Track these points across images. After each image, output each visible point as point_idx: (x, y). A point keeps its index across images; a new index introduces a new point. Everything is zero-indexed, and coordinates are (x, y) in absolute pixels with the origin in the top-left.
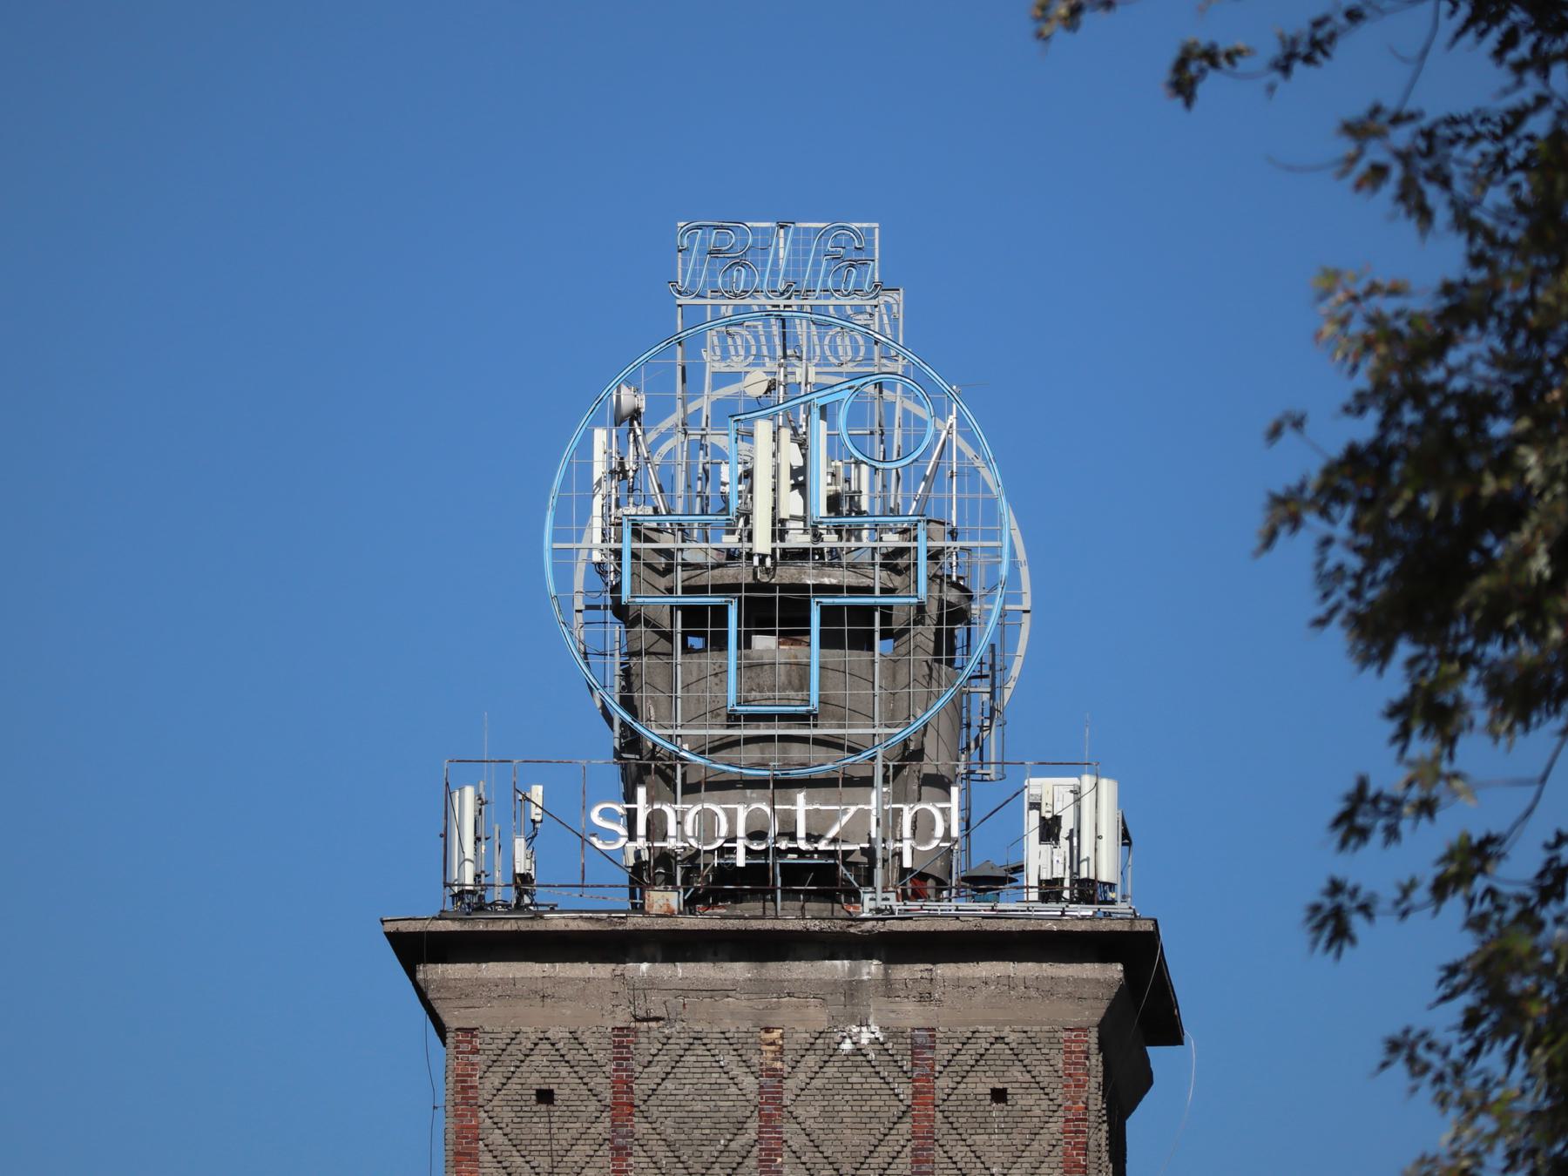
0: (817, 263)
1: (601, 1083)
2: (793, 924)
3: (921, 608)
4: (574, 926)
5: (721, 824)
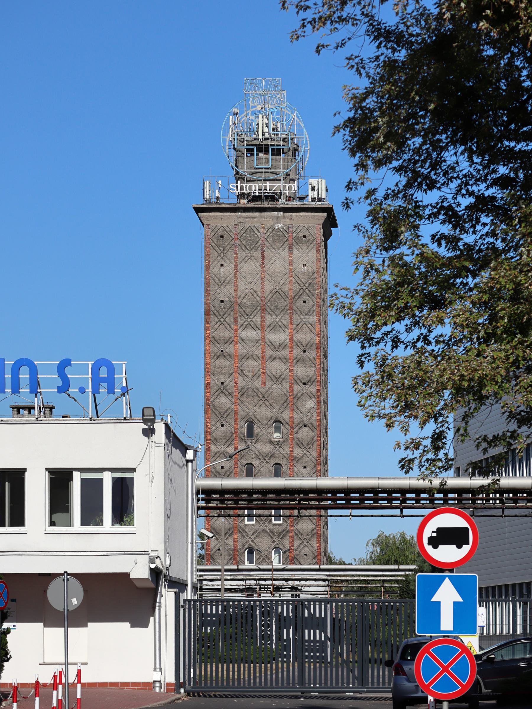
0: (270, 86)
1: (232, 235)
2: (267, 206)
3: (289, 149)
4: (227, 206)
5: (254, 188)
